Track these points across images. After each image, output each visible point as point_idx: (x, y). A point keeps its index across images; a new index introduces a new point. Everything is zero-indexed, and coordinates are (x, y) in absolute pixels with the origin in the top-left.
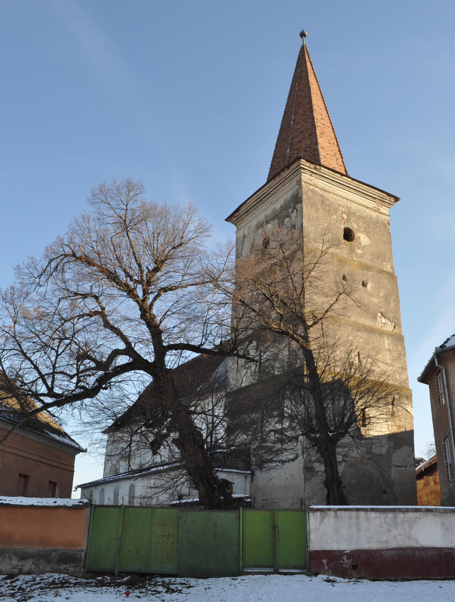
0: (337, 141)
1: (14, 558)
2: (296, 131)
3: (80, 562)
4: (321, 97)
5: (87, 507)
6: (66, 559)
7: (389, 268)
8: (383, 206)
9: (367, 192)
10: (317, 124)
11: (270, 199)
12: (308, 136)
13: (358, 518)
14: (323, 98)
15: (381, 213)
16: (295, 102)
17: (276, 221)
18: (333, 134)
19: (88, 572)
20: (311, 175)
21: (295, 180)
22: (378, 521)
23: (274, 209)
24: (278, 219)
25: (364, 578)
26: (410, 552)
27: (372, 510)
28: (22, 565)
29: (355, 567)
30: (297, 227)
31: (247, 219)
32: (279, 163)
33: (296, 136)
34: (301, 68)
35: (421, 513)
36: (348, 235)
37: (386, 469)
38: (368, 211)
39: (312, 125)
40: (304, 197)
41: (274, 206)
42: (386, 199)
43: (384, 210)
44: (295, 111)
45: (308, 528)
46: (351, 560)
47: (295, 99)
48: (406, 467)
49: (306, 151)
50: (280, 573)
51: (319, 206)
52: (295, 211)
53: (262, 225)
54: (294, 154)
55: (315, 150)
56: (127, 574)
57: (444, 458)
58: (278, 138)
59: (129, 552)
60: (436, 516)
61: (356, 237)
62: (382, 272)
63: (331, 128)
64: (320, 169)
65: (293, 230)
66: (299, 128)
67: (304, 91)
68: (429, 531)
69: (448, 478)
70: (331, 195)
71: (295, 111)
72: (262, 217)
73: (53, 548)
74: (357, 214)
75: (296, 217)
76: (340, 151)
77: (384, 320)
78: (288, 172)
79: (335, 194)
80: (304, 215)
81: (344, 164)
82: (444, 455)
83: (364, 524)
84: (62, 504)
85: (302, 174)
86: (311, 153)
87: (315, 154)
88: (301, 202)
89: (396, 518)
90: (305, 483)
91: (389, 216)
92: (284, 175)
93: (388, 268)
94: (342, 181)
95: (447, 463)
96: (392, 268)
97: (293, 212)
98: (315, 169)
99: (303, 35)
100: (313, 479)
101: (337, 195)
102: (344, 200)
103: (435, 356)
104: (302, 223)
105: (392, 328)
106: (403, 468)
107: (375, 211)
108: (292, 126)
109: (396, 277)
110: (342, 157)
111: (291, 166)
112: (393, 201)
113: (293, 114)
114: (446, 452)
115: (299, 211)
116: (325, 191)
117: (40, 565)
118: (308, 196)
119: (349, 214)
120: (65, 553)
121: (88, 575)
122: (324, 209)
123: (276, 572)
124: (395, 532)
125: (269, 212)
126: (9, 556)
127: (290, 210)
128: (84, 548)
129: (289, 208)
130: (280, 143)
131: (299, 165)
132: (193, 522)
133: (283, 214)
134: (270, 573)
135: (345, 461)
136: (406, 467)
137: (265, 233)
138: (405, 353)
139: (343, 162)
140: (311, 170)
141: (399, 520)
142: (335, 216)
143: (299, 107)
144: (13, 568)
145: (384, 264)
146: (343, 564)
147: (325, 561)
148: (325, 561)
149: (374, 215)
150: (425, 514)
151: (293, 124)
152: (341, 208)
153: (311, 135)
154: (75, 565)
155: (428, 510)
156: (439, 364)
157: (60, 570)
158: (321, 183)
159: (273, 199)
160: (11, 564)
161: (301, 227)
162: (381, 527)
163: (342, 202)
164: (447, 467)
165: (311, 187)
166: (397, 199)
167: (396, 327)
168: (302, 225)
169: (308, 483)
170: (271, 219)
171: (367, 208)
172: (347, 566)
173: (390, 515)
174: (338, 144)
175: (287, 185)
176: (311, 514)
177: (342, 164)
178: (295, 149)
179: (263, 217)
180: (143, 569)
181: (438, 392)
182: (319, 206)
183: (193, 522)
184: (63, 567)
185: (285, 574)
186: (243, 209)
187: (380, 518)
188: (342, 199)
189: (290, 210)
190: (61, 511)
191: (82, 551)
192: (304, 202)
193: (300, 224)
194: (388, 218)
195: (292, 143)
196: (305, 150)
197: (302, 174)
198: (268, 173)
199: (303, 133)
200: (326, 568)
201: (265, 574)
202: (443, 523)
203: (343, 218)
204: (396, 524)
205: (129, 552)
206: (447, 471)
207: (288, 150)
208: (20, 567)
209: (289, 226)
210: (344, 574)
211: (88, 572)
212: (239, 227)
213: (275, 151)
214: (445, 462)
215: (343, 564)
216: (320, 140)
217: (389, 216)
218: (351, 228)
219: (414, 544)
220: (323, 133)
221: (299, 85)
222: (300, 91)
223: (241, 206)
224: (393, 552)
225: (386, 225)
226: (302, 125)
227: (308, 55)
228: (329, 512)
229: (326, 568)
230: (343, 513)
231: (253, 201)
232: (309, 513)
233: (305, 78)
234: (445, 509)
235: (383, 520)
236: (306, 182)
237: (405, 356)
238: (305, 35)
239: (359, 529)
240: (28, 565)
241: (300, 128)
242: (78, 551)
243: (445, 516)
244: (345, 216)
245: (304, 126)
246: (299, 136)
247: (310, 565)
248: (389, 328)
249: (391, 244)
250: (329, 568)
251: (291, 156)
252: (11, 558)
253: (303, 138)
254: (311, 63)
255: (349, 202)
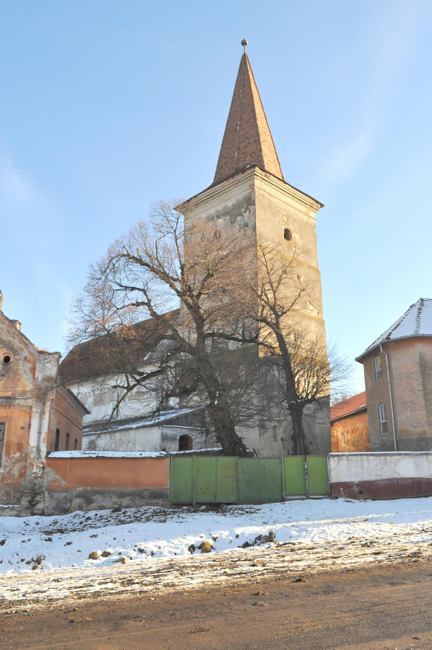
0: (275, 149)
1: (114, 497)
2: (243, 136)
3: (167, 497)
4: (261, 106)
5: (168, 457)
6: (156, 496)
7: (315, 264)
8: (311, 211)
9: (302, 198)
10: (261, 132)
11: (222, 196)
12: (253, 142)
13: (362, 460)
14: (263, 108)
15: (310, 217)
16: (240, 108)
17: (228, 218)
18: (272, 142)
19: (172, 504)
20: (261, 181)
21: (247, 184)
22: (375, 462)
23: (225, 207)
24: (230, 216)
25: (368, 499)
26: (396, 481)
27: (371, 455)
28: (121, 502)
29: (361, 492)
30: (249, 226)
31: (198, 211)
32: (226, 163)
33: (242, 141)
34: (244, 76)
35: (402, 456)
36: (287, 235)
37: (312, 426)
38: (301, 214)
39: (256, 132)
40: (257, 200)
41: (226, 203)
42: (314, 205)
43: (312, 214)
44: (241, 117)
45: (328, 468)
46: (359, 488)
47: (240, 106)
48: (325, 424)
49: (252, 157)
50: (312, 499)
51: (267, 209)
52: (248, 211)
53: (213, 219)
54: (241, 158)
55: (260, 156)
56: (203, 504)
57: (378, 418)
58: (223, 139)
59: (201, 489)
60: (411, 458)
61: (292, 237)
62: (310, 267)
63: (270, 136)
64: (269, 177)
65: (246, 228)
66: (244, 134)
67: (247, 99)
68: (407, 467)
69: (381, 432)
70: (276, 199)
71: (241, 117)
72: (212, 212)
73: (144, 488)
74: (294, 217)
75: (249, 217)
76: (277, 158)
77: (311, 307)
78: (242, 176)
79: (278, 199)
80: (257, 216)
81: (281, 171)
82: (378, 416)
83: (366, 464)
84: (147, 456)
85: (255, 179)
86: (256, 159)
87: (259, 160)
88: (254, 204)
89: (386, 460)
90: (260, 437)
91: (316, 219)
92: (237, 178)
93: (314, 265)
94: (284, 188)
95: (380, 422)
96: (317, 264)
97: (246, 212)
98: (266, 176)
99: (244, 43)
100: (265, 434)
101: (280, 200)
102: (285, 204)
103: (380, 345)
104: (255, 223)
105: (317, 314)
106: (323, 425)
107: (306, 215)
108: (238, 131)
109: (320, 272)
110: (279, 164)
111: (246, 172)
112: (319, 207)
113: (239, 119)
114: (379, 414)
115: (252, 212)
116: (271, 196)
117: (136, 501)
118: (260, 200)
119: (288, 217)
120: (155, 491)
121: (174, 506)
122: (270, 212)
123: (308, 498)
124: (386, 469)
125: (220, 208)
126: (109, 495)
127: (243, 210)
128: (168, 487)
129: (241, 208)
130: (226, 144)
131: (254, 172)
132: (247, 466)
133: (235, 212)
134: (305, 499)
135: (286, 420)
136: (325, 424)
137: (217, 226)
138: (325, 334)
139: (280, 169)
140: (262, 176)
141: (388, 461)
142: (278, 218)
143: (244, 113)
144: (114, 504)
145: (312, 260)
146: (353, 490)
147: (342, 489)
148: (342, 489)
149: (305, 218)
150: (404, 457)
151: (239, 130)
152: (282, 211)
153: (255, 142)
154: (163, 500)
155: (406, 454)
156: (383, 351)
157: (152, 503)
158: (268, 188)
159: (225, 197)
160: (111, 501)
161: (253, 226)
162: (377, 466)
163: (283, 206)
164: (380, 425)
165: (262, 192)
166: (322, 206)
167: (320, 313)
168: (255, 225)
169: (262, 437)
170: (222, 215)
171: (300, 212)
172: (356, 492)
173: (383, 458)
174: (276, 152)
175: (240, 187)
176: (331, 458)
177: (279, 170)
178: (242, 153)
179: (214, 211)
180: (213, 501)
181: (375, 370)
182: (267, 209)
183: (247, 466)
184: (154, 501)
185: (316, 499)
186: (193, 201)
187: (376, 460)
188: (283, 203)
189: (243, 210)
190: (147, 461)
191: (168, 489)
192: (256, 205)
193: (253, 224)
194: (315, 221)
195: (239, 147)
196: (251, 155)
197: (255, 179)
198: (215, 171)
199: (249, 139)
200: (343, 493)
201: (302, 499)
202: (415, 462)
203: (284, 220)
204: (386, 464)
205: (201, 489)
206: (380, 427)
207: (236, 153)
208: (120, 503)
209: (242, 223)
210: (354, 497)
211: (172, 504)
212: (187, 217)
213: (221, 151)
214: (378, 421)
215: (353, 490)
216: (263, 147)
217: (316, 219)
218: (289, 229)
219: (397, 476)
220: (265, 141)
221: (243, 92)
222: (244, 98)
223: (191, 199)
224: (385, 482)
225: (313, 227)
226: (247, 132)
227: (249, 64)
228: (343, 457)
229: (343, 493)
230: (352, 457)
231: (205, 196)
232: (329, 458)
233: (248, 87)
234: (416, 454)
235: (378, 461)
236: (258, 187)
237: (325, 337)
238: (246, 44)
239: (363, 468)
240: (126, 501)
241: (246, 134)
242: (164, 489)
243: (416, 458)
244: (285, 218)
245: (249, 133)
246: (245, 141)
247: (331, 492)
248: (314, 314)
249: (316, 243)
250: (345, 493)
251: (239, 159)
252: (111, 497)
253: (249, 143)
254: (252, 72)
255: (288, 206)
